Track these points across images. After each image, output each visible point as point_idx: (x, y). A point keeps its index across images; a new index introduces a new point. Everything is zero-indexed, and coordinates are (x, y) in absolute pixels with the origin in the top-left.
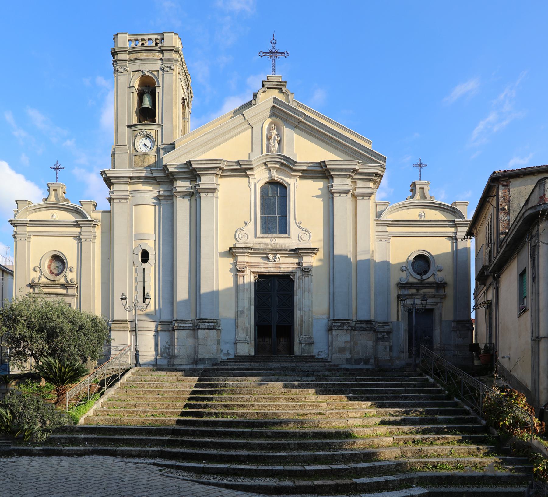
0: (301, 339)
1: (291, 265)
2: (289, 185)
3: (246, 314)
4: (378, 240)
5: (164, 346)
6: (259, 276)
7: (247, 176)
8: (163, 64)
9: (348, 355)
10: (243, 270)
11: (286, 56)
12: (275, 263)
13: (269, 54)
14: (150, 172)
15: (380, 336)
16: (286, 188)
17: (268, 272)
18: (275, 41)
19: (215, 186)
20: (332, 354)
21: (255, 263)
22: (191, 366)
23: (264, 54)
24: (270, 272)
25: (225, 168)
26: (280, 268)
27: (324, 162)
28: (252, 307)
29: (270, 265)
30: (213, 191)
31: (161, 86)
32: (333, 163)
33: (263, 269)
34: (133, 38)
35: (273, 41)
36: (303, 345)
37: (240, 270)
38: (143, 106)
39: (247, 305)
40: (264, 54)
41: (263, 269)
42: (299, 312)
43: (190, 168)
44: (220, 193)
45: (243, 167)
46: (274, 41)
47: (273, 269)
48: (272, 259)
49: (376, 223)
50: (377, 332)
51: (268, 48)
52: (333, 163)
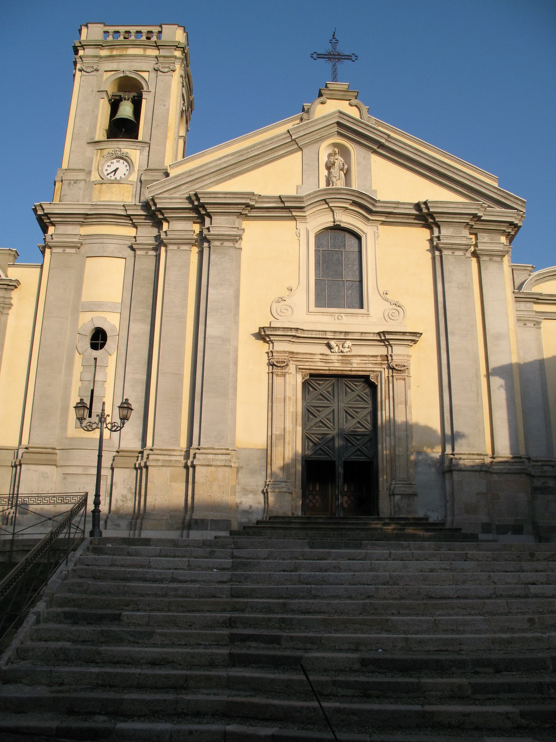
0: (392, 486)
1: (371, 359)
2: (366, 234)
3: (287, 440)
4: (521, 324)
5: (122, 496)
6: (311, 375)
7: (294, 218)
8: (157, 64)
9: (484, 518)
10: (403, 368)
11: (353, 59)
12: (342, 356)
13: (327, 56)
14: (123, 208)
15: (538, 483)
16: (358, 238)
17: (329, 370)
18: (337, 40)
19: (239, 233)
20: (453, 515)
21: (306, 354)
22: (173, 535)
23: (320, 56)
24: (332, 370)
25: (257, 205)
26: (351, 364)
27: (425, 203)
28: (299, 429)
29: (333, 358)
30: (236, 239)
31: (153, 91)
32: (440, 205)
33: (320, 364)
34: (111, 29)
35: (334, 41)
36: (397, 498)
37: (278, 365)
38: (117, 117)
39: (289, 426)
40: (320, 56)
41: (320, 364)
42: (388, 439)
43: (196, 203)
44: (245, 244)
45: (287, 204)
46: (334, 40)
47: (338, 365)
48: (336, 349)
49: (515, 297)
50: (533, 476)
51: (325, 47)
52: (440, 205)
